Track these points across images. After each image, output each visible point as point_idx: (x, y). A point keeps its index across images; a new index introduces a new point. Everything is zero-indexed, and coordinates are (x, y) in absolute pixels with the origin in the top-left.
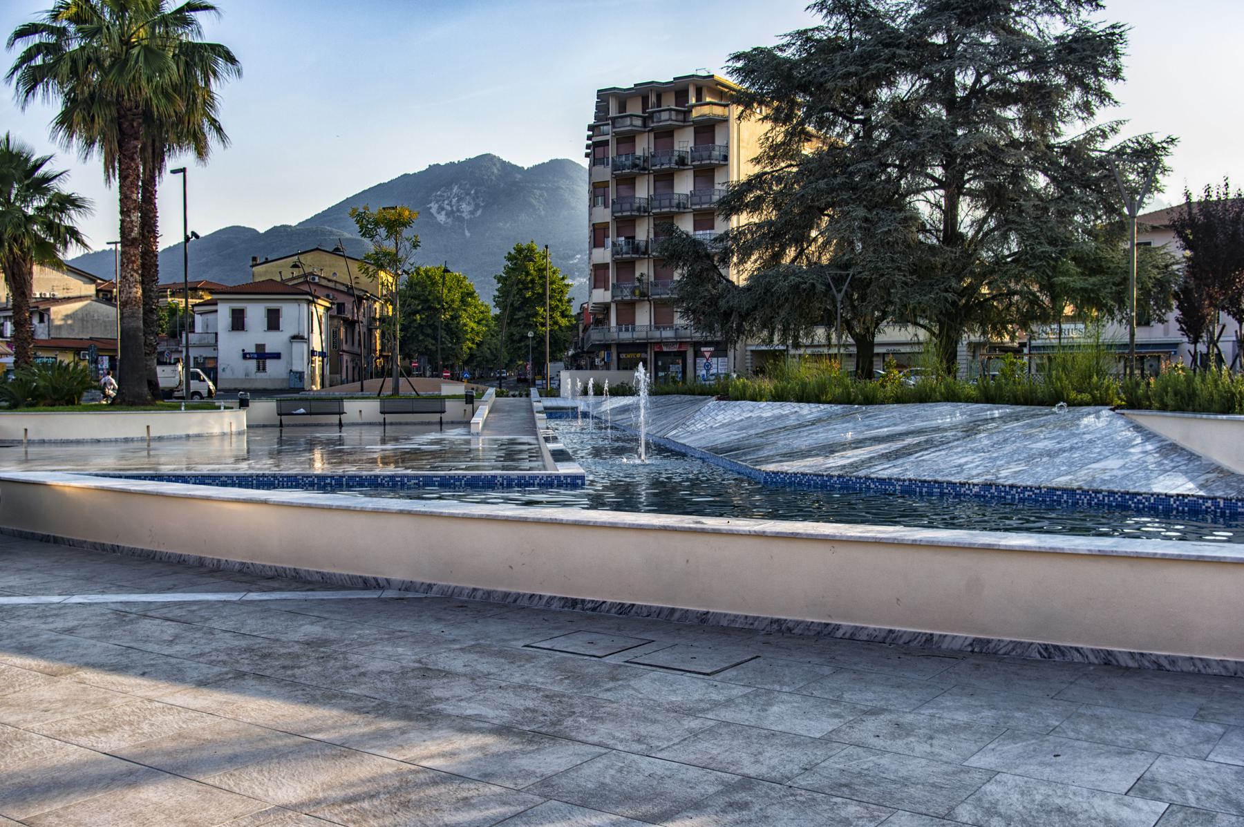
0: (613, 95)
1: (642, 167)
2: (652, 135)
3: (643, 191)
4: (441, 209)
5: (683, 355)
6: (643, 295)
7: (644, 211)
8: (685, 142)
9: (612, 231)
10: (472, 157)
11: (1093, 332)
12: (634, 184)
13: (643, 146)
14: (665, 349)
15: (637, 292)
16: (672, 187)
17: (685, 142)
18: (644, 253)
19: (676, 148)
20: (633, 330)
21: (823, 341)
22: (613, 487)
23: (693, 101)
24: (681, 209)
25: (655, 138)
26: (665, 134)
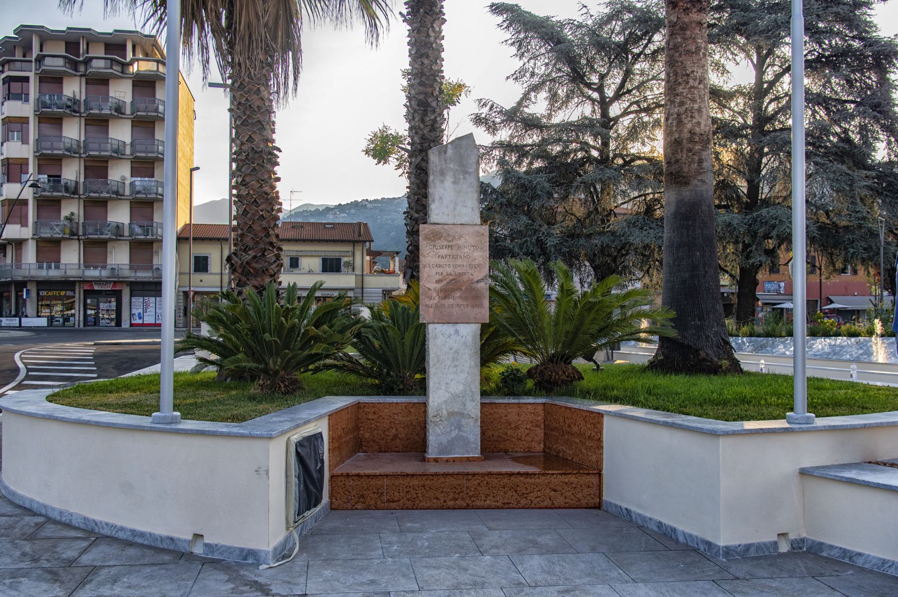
0: (36, 32)
1: (73, 108)
2: (84, 80)
3: (73, 131)
4: (549, 235)
5: (118, 295)
6: (73, 234)
7: (72, 152)
8: (122, 92)
9: (31, 168)
10: (371, 198)
11: (380, 552)
12: (61, 124)
13: (73, 88)
14: (96, 288)
15: (67, 231)
16: (107, 133)
17: (122, 92)
18: (74, 193)
19: (111, 94)
20: (57, 267)
21: (133, 322)
22: (418, 231)
23: (130, 56)
24: (118, 154)
25: (87, 83)
26: (99, 82)
